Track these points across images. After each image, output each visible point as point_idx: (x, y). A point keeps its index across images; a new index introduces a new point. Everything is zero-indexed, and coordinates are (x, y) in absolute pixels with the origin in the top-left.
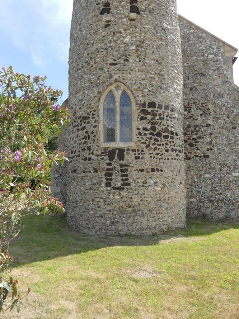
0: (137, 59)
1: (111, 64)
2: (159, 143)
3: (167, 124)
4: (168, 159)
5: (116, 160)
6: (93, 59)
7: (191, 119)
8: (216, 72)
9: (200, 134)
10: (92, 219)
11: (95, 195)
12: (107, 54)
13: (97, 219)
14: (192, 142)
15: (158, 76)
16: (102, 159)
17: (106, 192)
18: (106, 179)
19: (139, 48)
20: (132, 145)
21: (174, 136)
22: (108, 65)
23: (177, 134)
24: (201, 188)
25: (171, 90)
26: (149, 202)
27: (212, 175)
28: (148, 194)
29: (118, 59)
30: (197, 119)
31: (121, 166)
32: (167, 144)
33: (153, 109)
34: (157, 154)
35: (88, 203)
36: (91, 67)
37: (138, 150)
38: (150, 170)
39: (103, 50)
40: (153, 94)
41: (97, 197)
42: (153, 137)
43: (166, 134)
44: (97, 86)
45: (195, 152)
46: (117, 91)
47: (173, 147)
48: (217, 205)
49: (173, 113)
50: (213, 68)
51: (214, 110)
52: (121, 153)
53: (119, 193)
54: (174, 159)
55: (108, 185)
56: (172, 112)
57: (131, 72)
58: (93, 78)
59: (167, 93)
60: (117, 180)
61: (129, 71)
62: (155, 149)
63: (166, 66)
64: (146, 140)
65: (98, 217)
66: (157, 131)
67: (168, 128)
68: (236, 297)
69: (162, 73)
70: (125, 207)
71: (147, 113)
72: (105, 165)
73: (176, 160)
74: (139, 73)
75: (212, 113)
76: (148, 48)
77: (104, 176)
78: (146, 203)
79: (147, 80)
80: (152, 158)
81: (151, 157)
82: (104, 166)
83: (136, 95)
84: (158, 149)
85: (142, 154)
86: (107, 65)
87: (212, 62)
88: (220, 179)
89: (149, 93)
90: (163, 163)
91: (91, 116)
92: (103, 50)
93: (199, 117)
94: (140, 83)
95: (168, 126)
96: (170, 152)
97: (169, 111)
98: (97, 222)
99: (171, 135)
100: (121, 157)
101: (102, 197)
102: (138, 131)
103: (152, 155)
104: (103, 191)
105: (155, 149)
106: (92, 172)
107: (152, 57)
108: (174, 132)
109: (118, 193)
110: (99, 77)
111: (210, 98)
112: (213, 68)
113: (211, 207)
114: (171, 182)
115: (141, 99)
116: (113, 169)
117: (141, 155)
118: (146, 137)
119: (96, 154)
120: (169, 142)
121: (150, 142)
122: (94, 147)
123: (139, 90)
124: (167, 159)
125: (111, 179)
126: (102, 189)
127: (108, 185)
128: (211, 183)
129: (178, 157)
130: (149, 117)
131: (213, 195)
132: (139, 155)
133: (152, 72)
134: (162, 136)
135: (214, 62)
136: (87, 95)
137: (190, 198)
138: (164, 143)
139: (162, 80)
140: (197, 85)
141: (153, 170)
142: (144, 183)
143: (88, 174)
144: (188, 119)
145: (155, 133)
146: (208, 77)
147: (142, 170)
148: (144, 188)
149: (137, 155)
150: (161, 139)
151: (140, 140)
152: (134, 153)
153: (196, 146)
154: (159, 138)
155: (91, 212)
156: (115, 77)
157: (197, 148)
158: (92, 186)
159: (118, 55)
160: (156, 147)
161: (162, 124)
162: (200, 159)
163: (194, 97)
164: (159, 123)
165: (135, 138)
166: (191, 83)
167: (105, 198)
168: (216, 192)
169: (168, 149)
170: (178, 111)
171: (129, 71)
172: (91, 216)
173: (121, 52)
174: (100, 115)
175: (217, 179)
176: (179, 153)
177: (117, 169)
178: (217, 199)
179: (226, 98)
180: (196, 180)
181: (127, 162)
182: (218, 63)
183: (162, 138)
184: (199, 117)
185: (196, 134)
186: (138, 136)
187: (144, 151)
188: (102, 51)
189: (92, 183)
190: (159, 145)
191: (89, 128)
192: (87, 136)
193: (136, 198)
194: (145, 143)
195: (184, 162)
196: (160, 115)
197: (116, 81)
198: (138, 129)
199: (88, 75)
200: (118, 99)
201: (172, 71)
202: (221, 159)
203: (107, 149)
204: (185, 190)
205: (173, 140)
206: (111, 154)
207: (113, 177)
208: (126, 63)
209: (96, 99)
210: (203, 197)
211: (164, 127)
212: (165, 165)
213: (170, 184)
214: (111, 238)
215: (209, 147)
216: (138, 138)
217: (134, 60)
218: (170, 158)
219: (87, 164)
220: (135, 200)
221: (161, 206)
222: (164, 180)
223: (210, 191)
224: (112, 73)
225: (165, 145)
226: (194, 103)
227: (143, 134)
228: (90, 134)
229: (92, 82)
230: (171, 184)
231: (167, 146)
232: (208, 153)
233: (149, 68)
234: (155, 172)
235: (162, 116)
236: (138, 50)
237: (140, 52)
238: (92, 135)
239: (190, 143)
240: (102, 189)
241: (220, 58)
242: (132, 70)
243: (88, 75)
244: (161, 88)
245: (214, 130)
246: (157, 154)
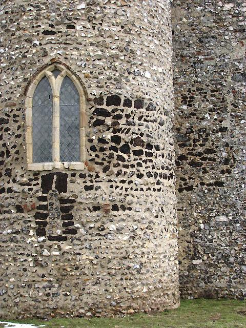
0: (89, 25)
1: (46, 33)
2: (126, 163)
3: (140, 132)
4: (142, 190)
5: (53, 191)
6: (14, 22)
8: (238, 35)
9: (208, 145)
10: (13, 291)
11: (18, 250)
12: (39, 15)
13: (21, 290)
14: (195, 159)
15: (125, 53)
16: (31, 190)
17: (36, 245)
18: (37, 223)
19: (93, 7)
20: (78, 165)
21: (154, 150)
22: (40, 33)
23: (157, 148)
24: (211, 241)
25: (148, 75)
26: (109, 261)
27: (231, 218)
28: (107, 247)
29: (57, 25)
30: (203, 119)
31: (62, 201)
32: (139, 165)
33: (116, 107)
34: (123, 182)
35: (7, 264)
36: (12, 35)
37: (90, 176)
38: (110, 208)
39: (32, 8)
40: (115, 83)
41: (21, 254)
42: (116, 154)
43: (138, 148)
44: (23, 69)
45: (200, 177)
46: (56, 77)
47: (150, 170)
48: (239, 270)
49: (150, 113)
50: (231, 28)
51: (233, 102)
52: (62, 180)
53: (59, 246)
54: (152, 189)
56: (148, 112)
57: (79, 46)
58: (15, 54)
59: (140, 79)
60: (56, 224)
61: (75, 45)
62: (118, 174)
63: (139, 35)
64: (104, 159)
65: (24, 287)
66: (122, 143)
67: (142, 138)
68: (144, 302)
69: (132, 46)
70: (69, 269)
71: (106, 114)
72: (35, 200)
73: (156, 191)
74: (92, 48)
75: (230, 107)
76: (107, 7)
77: (33, 219)
78: (104, 262)
79: (104, 60)
80: (114, 188)
81: (111, 187)
82: (34, 201)
83: (86, 85)
84: (123, 172)
85: (96, 182)
86: (38, 34)
87: (230, 16)
89: (108, 82)
90: (133, 196)
91: (11, 119)
92: (32, 8)
93: (207, 116)
94: (95, 66)
95: (142, 134)
96: (145, 178)
97: (143, 110)
98: (21, 296)
99: (147, 151)
100: (62, 186)
101: (29, 253)
102: (90, 145)
103: (113, 183)
104: (31, 244)
105: (118, 174)
106: (13, 211)
107: (114, 22)
108: (153, 144)
109: (56, 247)
110: (26, 54)
111: (226, 81)
113: (228, 274)
114: (147, 228)
115: (94, 91)
116: (49, 207)
117: (94, 183)
118: (104, 154)
119: (19, 183)
120: (143, 161)
121: (109, 162)
122: (17, 171)
123: (92, 76)
124: (139, 189)
125: (45, 224)
126: (30, 239)
127: (40, 232)
128: (228, 231)
129: (161, 186)
130: (109, 121)
131: (232, 252)
132: (92, 184)
133: (114, 47)
134: (131, 152)
135: (233, 17)
136: (5, 82)
137: (193, 259)
138: (135, 163)
139: (131, 59)
140: (203, 57)
141: (115, 208)
142: (100, 229)
143: (7, 215)
144: (187, 118)
145: (119, 147)
146: (222, 43)
147: (96, 208)
148: (100, 237)
149: (89, 184)
150: (129, 156)
151: (94, 159)
152: (83, 180)
153: (203, 166)
154: (125, 156)
155: (12, 280)
156: (52, 54)
157: (204, 169)
158: (14, 235)
159: (58, 18)
160: (121, 170)
161: (131, 132)
162: (209, 190)
163: (199, 80)
164: (125, 131)
165: (85, 156)
166: (193, 54)
167: (35, 254)
168: (237, 248)
169: (142, 172)
170: (162, 109)
171: (75, 45)
172: (12, 286)
173: (62, 14)
174: (26, 117)
175: (238, 225)
176: (162, 180)
177: (54, 206)
178: (238, 259)
180: (202, 226)
181: (71, 194)
182: (241, 18)
183: (132, 155)
184: (207, 116)
185: (201, 145)
186: (90, 152)
187: (99, 177)
188: (30, 10)
189: (14, 231)
190: (126, 167)
191: (9, 139)
192: (5, 152)
193: (87, 254)
194: (102, 164)
195: (173, 196)
196: (128, 116)
197: (53, 61)
198: (91, 141)
199: (7, 49)
200: (56, 91)
201: (149, 42)
203: (39, 174)
204: (175, 242)
205: (150, 158)
206: (47, 180)
207: (48, 220)
208: (70, 30)
209: (20, 90)
210: (215, 257)
211: (135, 137)
212: (135, 199)
213: (144, 231)
215: (225, 167)
216: (91, 155)
217: (84, 27)
218: (145, 188)
219: (5, 199)
220: (84, 257)
221: (129, 268)
222: (132, 225)
223: (227, 246)
224: (47, 47)
225: (136, 166)
226: (198, 89)
227: (98, 149)
228: (9, 148)
229: (13, 61)
230: (147, 230)
231: (140, 168)
232: (223, 178)
233: (108, 40)
234: (118, 210)
235: (131, 120)
236: (90, 10)
237: (93, 14)
238: (14, 150)
239: (192, 160)
240: (29, 240)
242: (81, 44)
243: (7, 49)
244: (129, 73)
245: (234, 137)
246: (123, 182)
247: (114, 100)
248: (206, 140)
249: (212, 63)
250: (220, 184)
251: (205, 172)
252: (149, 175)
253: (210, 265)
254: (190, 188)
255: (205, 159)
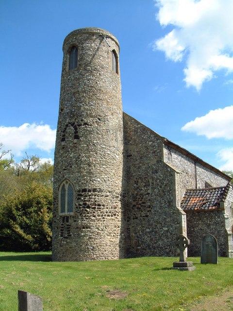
1: (64, 170)
7: (138, 189)
9: (143, 200)
20: (72, 214)
24: (144, 239)
31: (68, 225)
32: (94, 212)
55: (62, 236)
88: (156, 232)
94: (78, 179)
112: (151, 152)
127: (62, 236)
141: (84, 228)
179: (159, 173)
180: (141, 233)
194: (79, 213)
198: (76, 205)
202: (156, 218)
214: (130, 265)
215: (149, 209)
236: (77, 160)
241: (156, 144)
247: (85, 190)
248: (142, 198)
249: (145, 166)
250: (147, 216)
251: (142, 211)
252: (99, 216)
253: (144, 249)
254: (137, 218)
255: (142, 206)
